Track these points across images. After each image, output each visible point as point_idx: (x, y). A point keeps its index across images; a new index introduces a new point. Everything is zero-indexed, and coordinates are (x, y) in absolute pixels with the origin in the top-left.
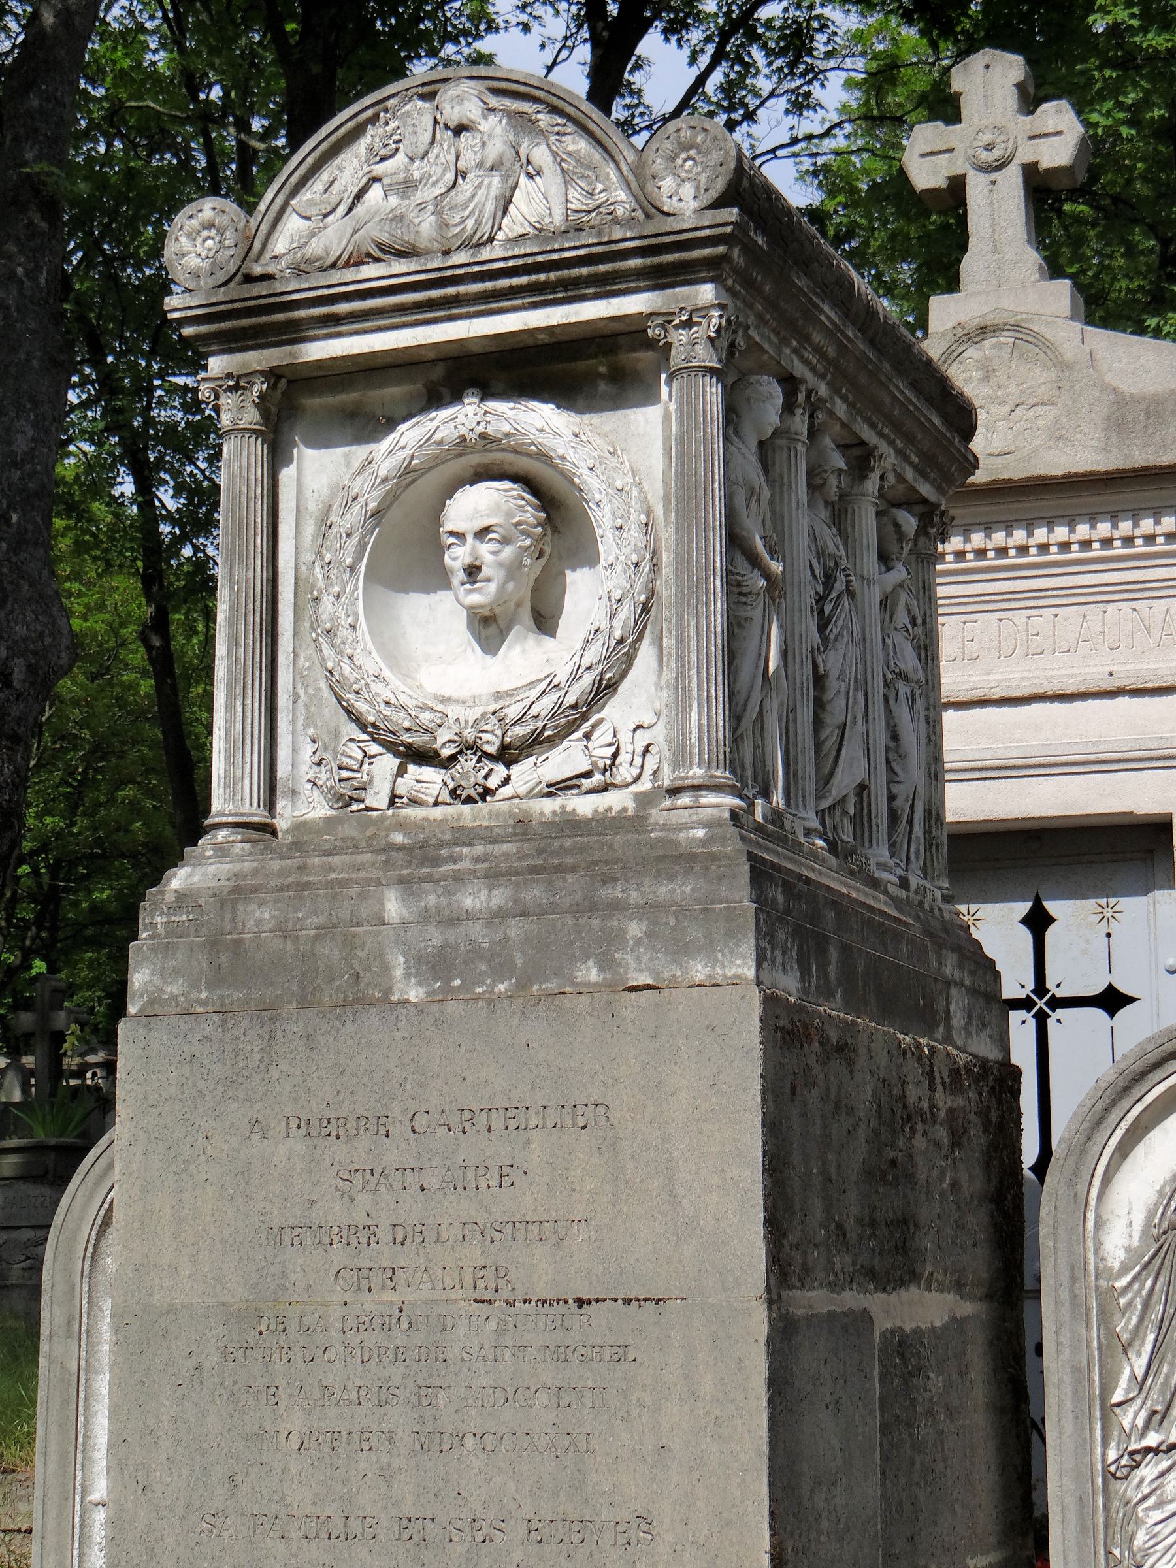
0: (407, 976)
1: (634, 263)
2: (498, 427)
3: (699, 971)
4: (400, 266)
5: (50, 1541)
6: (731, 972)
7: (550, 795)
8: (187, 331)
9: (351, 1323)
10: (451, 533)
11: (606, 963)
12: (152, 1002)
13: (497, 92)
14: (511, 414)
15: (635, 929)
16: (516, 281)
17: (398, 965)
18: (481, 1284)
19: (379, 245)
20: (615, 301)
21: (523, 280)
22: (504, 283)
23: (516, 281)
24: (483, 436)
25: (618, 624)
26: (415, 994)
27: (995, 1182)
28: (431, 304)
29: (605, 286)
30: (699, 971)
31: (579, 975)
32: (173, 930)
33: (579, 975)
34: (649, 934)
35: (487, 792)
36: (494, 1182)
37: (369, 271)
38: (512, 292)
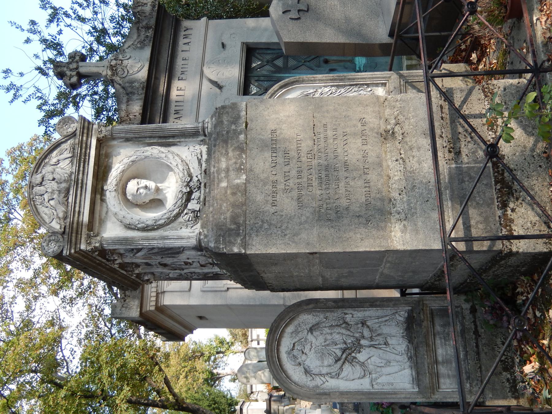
0: (240, 179)
1: (85, 138)
2: (114, 183)
3: (243, 113)
4: (71, 192)
5: (383, 396)
6: (244, 107)
7: (201, 166)
8: (73, 251)
9: (320, 188)
10: (137, 191)
11: (240, 133)
12: (242, 246)
13: (37, 172)
14: (112, 178)
15: (233, 127)
16: (82, 166)
17: (238, 181)
18: (311, 157)
19: (65, 197)
20: (92, 146)
21: (82, 164)
22: (81, 169)
23: (82, 166)
24: (116, 185)
25: (165, 151)
26: (244, 177)
27: (293, 387)
28: (82, 187)
29: (88, 147)
30: (243, 113)
31: (243, 139)
32: (224, 243)
33: (243, 139)
34: (235, 124)
35: (198, 180)
36: (288, 155)
37: (70, 200)
38: (84, 167)
